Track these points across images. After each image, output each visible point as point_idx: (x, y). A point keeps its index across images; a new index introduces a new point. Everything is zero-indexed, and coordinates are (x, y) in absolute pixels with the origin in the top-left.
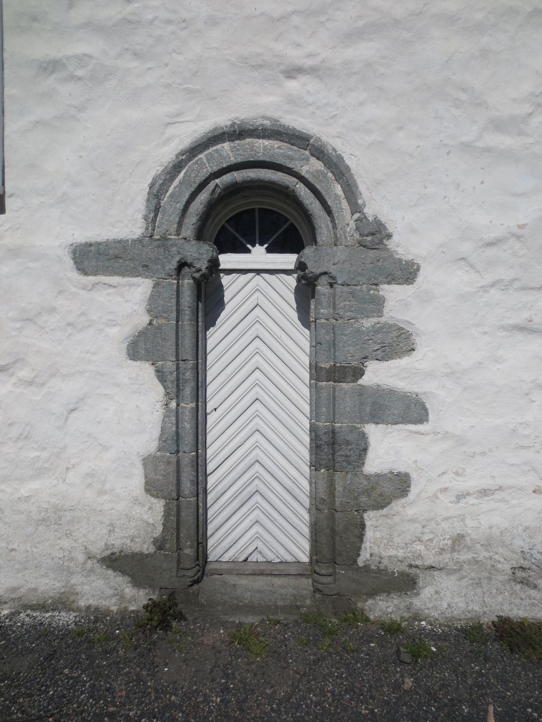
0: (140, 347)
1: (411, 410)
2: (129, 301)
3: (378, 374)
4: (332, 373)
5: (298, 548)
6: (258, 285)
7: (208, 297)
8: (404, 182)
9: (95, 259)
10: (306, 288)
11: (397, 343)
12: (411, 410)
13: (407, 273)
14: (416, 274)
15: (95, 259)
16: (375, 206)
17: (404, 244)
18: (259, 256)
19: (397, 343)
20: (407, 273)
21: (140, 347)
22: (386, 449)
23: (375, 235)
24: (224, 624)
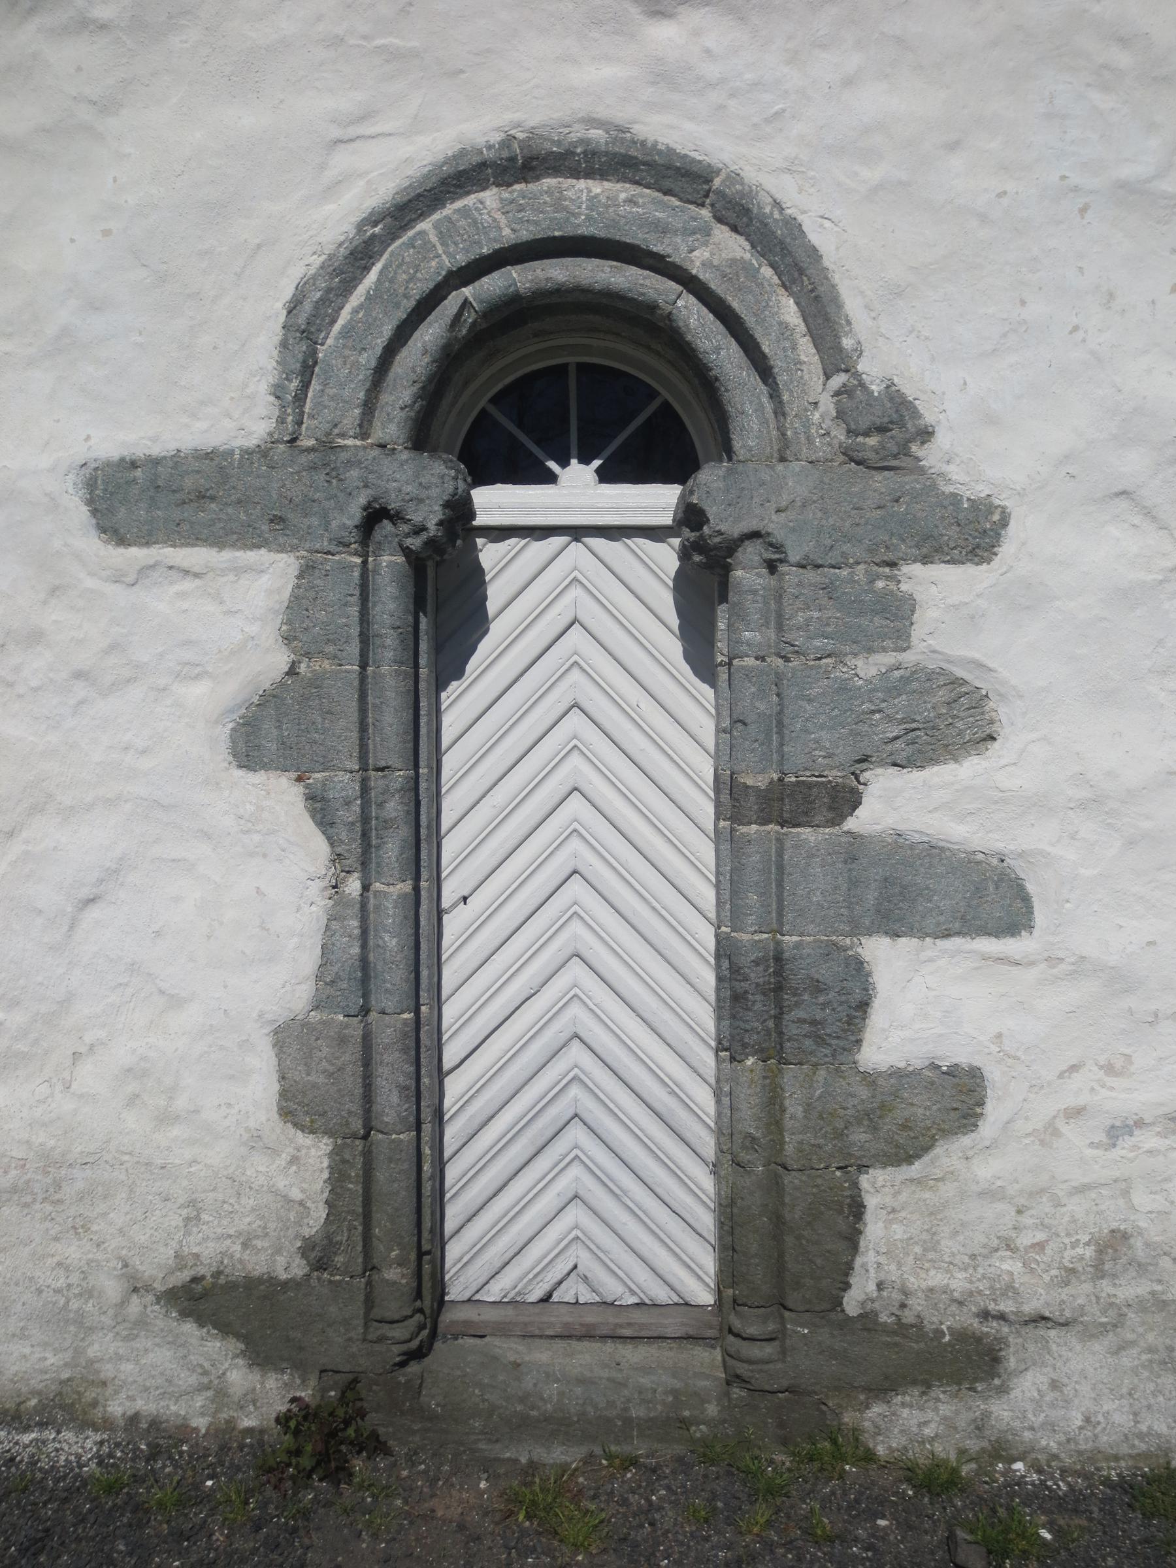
0: (264, 735)
1: (987, 900)
2: (234, 613)
3: (894, 803)
4: (776, 800)
5: (689, 1271)
6: (577, 565)
7: (445, 602)
8: (948, 276)
9: (148, 502)
10: (705, 574)
11: (948, 720)
12: (987, 900)
13: (973, 533)
14: (998, 535)
15: (148, 502)
16: (890, 353)
17: (963, 458)
18: (578, 490)
19: (948, 720)
20: (973, 533)
21: (264, 735)
22: (921, 1002)
23: (887, 431)
24: (488, 1466)
